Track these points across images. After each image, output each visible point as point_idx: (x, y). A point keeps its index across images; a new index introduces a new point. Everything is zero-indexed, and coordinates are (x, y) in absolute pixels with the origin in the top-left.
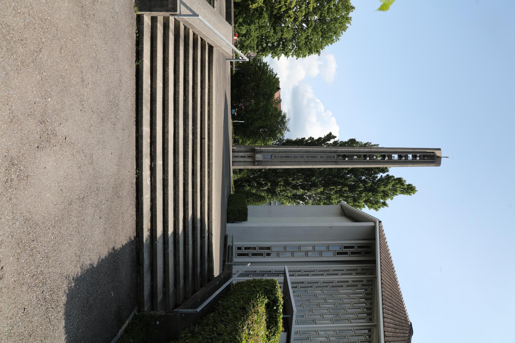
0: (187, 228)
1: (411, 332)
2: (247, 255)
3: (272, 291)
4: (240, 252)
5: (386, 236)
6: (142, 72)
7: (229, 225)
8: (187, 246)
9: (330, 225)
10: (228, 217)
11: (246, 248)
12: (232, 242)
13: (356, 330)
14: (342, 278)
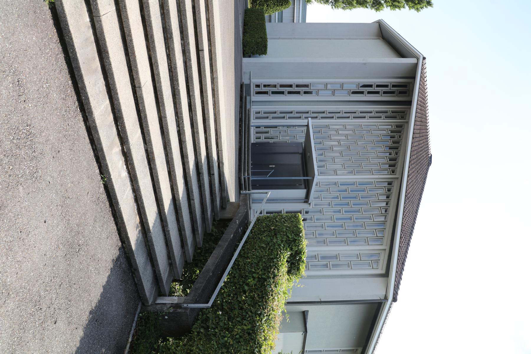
0: (189, 183)
1: (430, 163)
2: (266, 93)
3: (295, 240)
4: (258, 90)
5: (427, 74)
6: (65, 17)
7: (246, 60)
8: (192, 201)
9: (364, 62)
10: (244, 51)
11: (265, 86)
12: (250, 79)
13: (377, 182)
14: (369, 122)
